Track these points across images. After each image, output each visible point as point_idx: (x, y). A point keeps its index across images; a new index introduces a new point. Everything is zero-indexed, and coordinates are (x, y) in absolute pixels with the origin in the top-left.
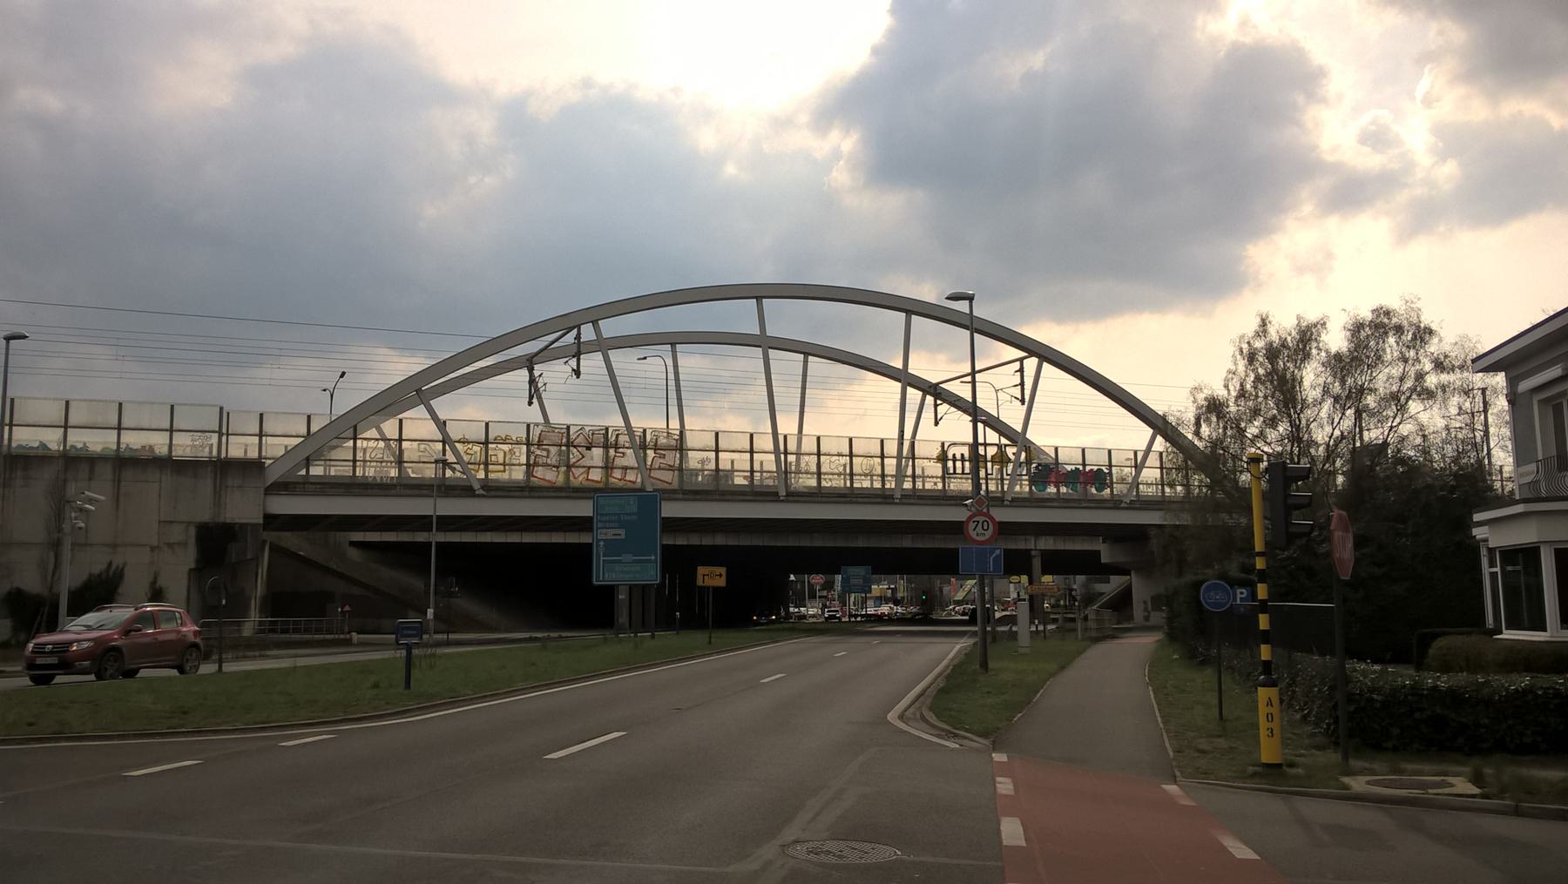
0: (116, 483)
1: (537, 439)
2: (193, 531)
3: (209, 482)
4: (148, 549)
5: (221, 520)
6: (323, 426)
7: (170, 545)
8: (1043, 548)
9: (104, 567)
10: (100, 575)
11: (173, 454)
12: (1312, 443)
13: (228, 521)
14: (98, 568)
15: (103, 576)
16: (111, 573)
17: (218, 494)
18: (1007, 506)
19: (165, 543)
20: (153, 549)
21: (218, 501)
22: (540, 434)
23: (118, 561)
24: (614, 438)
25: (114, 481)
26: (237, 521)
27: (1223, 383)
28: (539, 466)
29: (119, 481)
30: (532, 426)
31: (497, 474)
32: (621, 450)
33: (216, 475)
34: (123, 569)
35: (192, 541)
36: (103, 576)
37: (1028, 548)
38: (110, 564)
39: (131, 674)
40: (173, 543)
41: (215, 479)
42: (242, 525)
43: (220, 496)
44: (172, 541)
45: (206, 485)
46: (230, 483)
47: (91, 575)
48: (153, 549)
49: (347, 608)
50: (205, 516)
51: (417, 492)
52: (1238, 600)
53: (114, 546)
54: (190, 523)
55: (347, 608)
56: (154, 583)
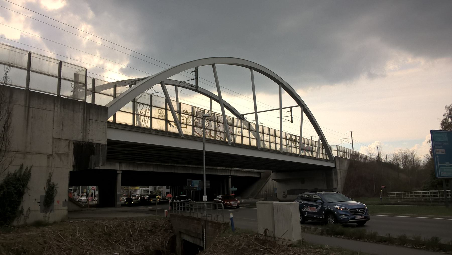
0: (27, 108)
1: (196, 114)
2: (72, 147)
3: (81, 115)
4: (46, 157)
5: (87, 140)
6: (84, 94)
7: (59, 155)
8: (232, 175)
9: (18, 168)
10: (15, 175)
11: (61, 93)
12: (371, 144)
13: (91, 141)
14: (13, 169)
15: (18, 175)
16: (23, 172)
17: (85, 122)
18: (300, 157)
19: (56, 153)
20: (49, 157)
21: (85, 129)
22: (197, 112)
23: (27, 164)
24: (217, 117)
25: (26, 106)
26: (95, 142)
27: (442, 118)
28: (196, 127)
29: (29, 107)
30: (194, 107)
31: (137, 131)
32: (219, 123)
33: (84, 110)
34: (30, 171)
35: (71, 153)
36: (18, 175)
37: (229, 175)
38: (22, 166)
39: (205, 253)
40: (61, 154)
41: (84, 113)
42: (97, 144)
43: (86, 124)
44: (60, 152)
45: (79, 117)
46: (91, 117)
47: (9, 175)
48: (49, 157)
49: (450, 197)
50: (78, 137)
51: (158, 133)
52: (231, 192)
53: (25, 153)
54: (70, 140)
55: (450, 197)
56: (49, 181)
